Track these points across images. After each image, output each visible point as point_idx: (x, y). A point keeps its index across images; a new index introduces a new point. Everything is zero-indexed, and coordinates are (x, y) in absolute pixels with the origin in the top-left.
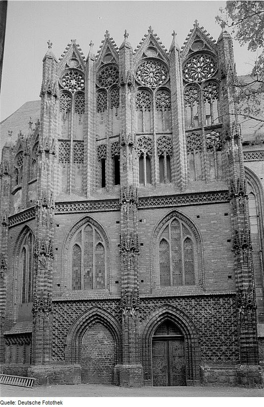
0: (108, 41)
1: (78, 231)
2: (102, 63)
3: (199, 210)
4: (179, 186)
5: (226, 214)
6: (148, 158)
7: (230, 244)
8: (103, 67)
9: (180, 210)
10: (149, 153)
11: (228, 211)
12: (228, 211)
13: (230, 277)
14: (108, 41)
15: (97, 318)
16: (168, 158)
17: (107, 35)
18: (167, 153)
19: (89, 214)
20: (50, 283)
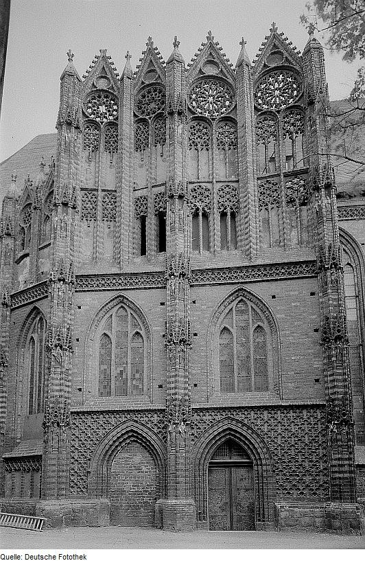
0: (151, 52)
1: (108, 315)
2: (143, 83)
3: (274, 288)
4: (248, 255)
5: (312, 294)
6: (205, 216)
7: (318, 335)
8: (143, 88)
9: (248, 287)
10: (206, 209)
11: (316, 289)
12: (316, 289)
13: (317, 381)
14: (151, 52)
15: (230, 434)
16: (233, 215)
17: (150, 43)
18: (231, 209)
19: (123, 292)
20: (68, 386)
